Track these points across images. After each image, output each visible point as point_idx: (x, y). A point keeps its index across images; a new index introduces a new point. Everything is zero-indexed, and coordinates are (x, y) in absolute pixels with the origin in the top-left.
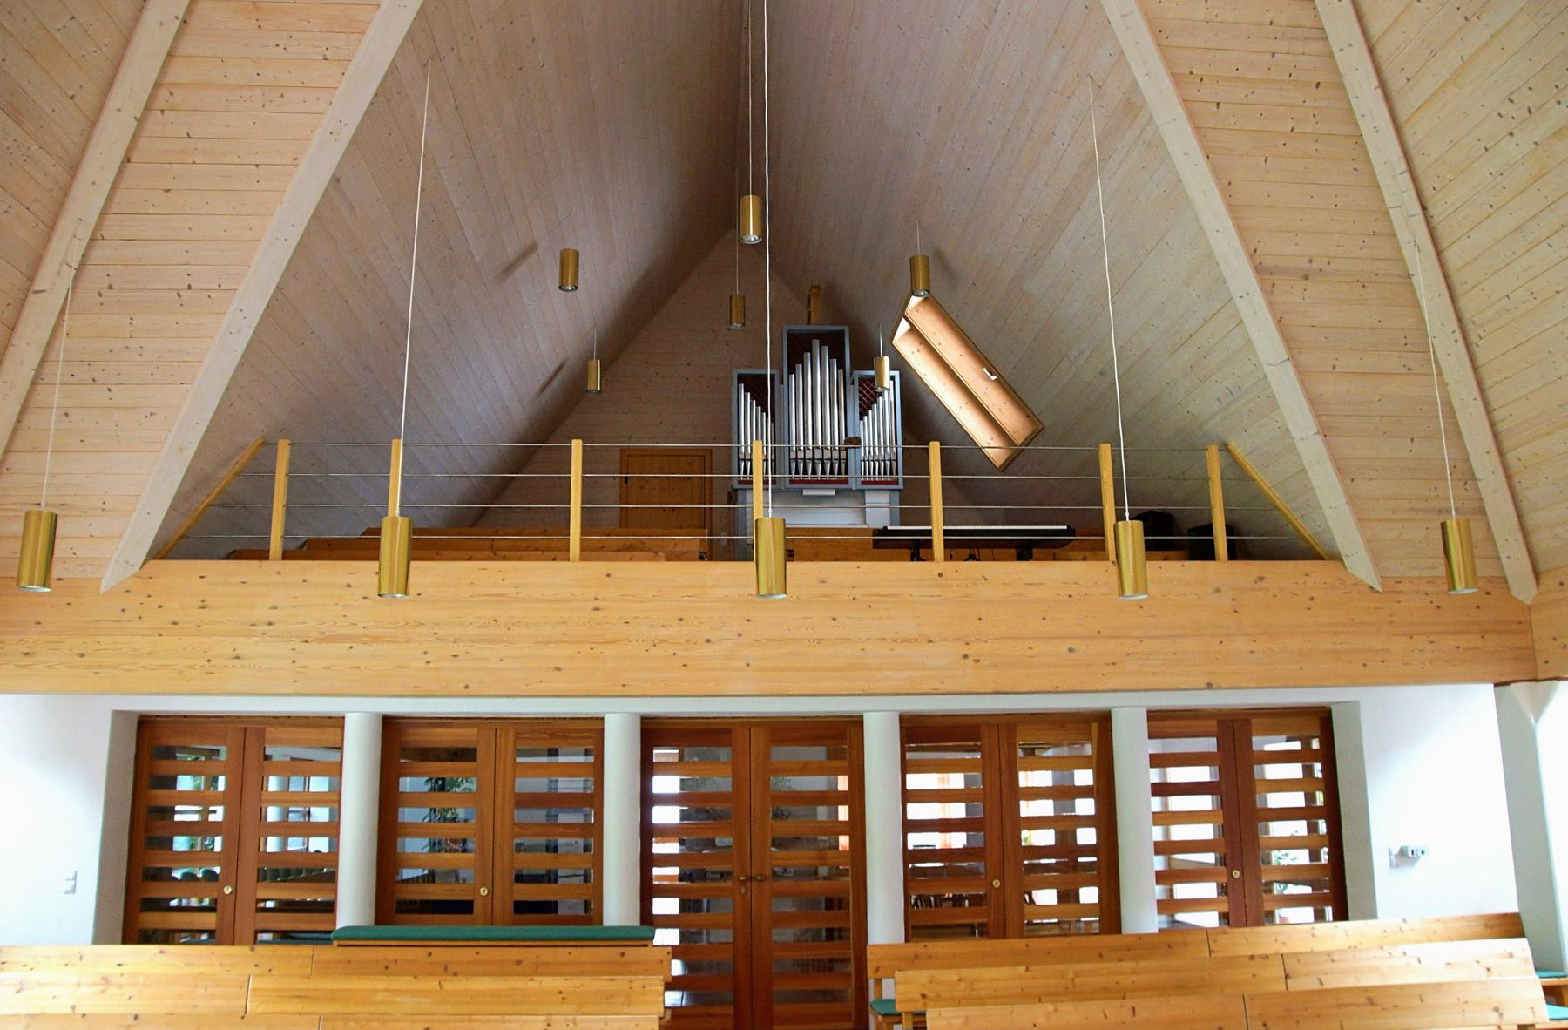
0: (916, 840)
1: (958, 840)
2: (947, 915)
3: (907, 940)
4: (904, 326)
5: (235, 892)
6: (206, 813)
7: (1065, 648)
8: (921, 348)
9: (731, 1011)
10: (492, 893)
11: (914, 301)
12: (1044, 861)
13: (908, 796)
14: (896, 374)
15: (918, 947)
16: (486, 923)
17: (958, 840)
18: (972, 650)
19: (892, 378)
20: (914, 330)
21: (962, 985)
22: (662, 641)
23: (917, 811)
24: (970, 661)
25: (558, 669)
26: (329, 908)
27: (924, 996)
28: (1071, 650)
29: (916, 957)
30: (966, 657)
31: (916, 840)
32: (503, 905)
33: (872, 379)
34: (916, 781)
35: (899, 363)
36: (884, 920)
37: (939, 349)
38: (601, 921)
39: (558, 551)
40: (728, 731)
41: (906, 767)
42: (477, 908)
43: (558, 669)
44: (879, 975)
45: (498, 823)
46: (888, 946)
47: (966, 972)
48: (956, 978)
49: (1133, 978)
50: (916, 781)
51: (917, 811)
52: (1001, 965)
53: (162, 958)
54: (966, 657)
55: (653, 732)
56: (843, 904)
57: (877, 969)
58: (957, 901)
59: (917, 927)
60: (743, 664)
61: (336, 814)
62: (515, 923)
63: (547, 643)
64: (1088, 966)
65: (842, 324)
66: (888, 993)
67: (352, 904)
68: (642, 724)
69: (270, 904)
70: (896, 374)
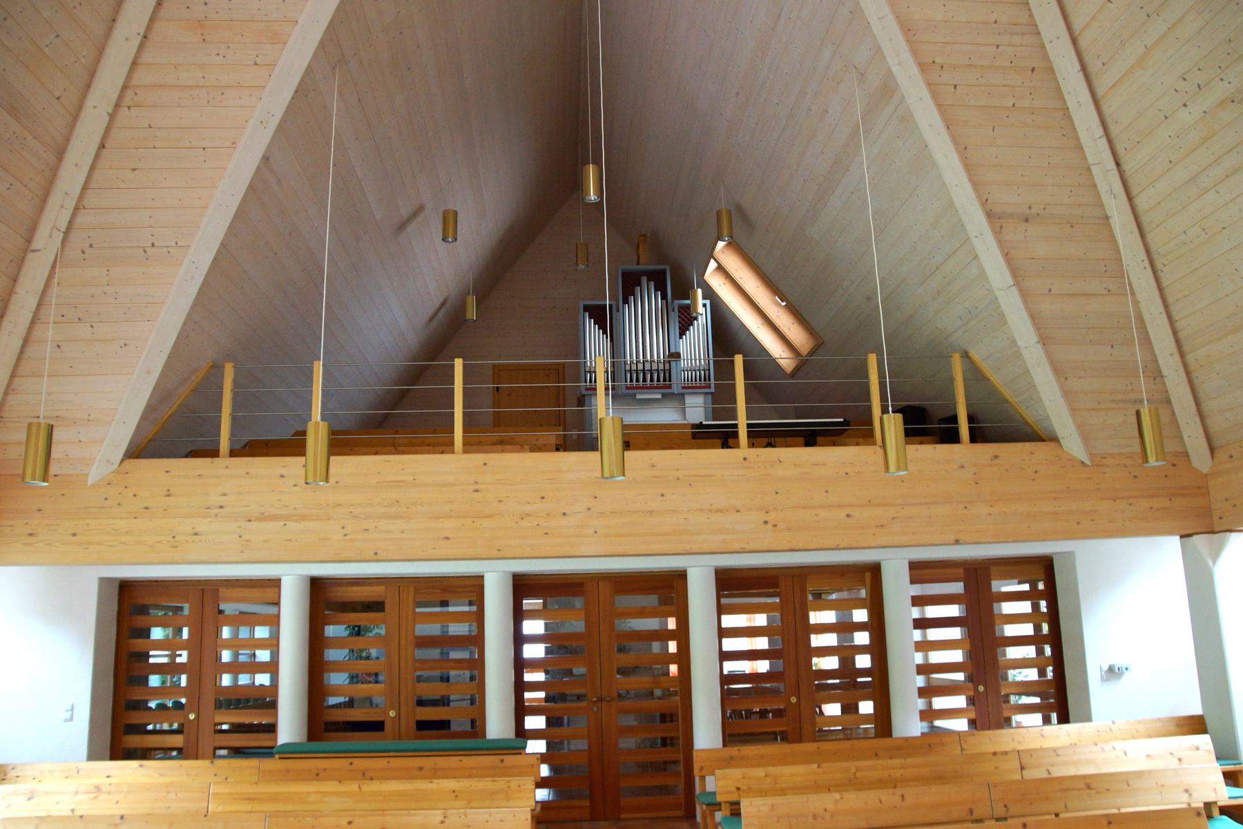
0: (730, 667)
3: (725, 745)
4: (713, 265)
6: (173, 656)
7: (843, 514)
8: (727, 282)
10: (399, 714)
11: (721, 244)
13: (723, 633)
14: (708, 302)
15: (733, 751)
17: (763, 666)
18: (771, 517)
19: (704, 305)
20: (720, 268)
21: (768, 780)
22: (528, 515)
23: (730, 644)
24: (769, 526)
25: (447, 538)
27: (738, 789)
28: (848, 516)
29: (732, 758)
30: (766, 522)
31: (730, 667)
32: (408, 724)
33: (688, 307)
34: (729, 621)
35: (710, 294)
36: (706, 730)
37: (741, 282)
39: (445, 446)
41: (721, 610)
42: (388, 727)
43: (447, 538)
46: (709, 750)
47: (773, 770)
48: (763, 774)
50: (729, 621)
51: (730, 644)
54: (766, 522)
56: (674, 718)
57: (702, 768)
59: (731, 736)
60: (592, 532)
62: (416, 738)
63: (438, 518)
65: (664, 263)
69: (225, 727)
70: (708, 302)
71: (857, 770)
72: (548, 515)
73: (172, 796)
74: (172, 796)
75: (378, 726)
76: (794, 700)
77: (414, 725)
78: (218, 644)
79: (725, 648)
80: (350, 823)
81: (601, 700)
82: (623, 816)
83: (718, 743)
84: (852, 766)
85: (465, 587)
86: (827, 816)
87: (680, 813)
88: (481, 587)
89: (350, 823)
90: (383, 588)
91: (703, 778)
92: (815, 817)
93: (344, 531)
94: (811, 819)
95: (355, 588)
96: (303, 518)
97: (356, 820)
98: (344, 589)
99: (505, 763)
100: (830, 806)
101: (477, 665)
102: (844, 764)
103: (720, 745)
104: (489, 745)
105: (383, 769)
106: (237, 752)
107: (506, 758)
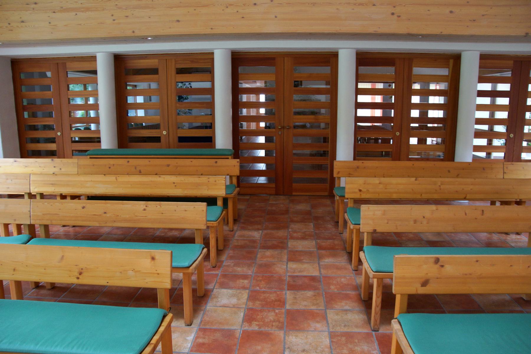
0: (362, 113)
1: (378, 113)
2: (372, 147)
3: (355, 159)
5: (62, 134)
6: (87, 100)
7: (447, 11)
9: (274, 186)
10: (168, 133)
12: (436, 125)
13: (359, 92)
15: (359, 163)
16: (167, 148)
17: (378, 113)
18: (397, 10)
21: (381, 186)
22: (231, 5)
23: (362, 99)
24: (395, 17)
25: (178, 21)
26: (98, 140)
27: (360, 191)
28: (451, 12)
29: (358, 167)
30: (393, 14)
31: (362, 113)
32: (174, 140)
34: (361, 86)
36: (344, 150)
38: (215, 147)
40: (274, 59)
41: (359, 78)
42: (162, 140)
43: (178, 21)
44: (339, 176)
45: (169, 102)
46: (345, 162)
47: (383, 180)
48: (378, 182)
49: (471, 187)
50: (361, 86)
51: (362, 99)
52: (403, 176)
53: (15, 164)
54: (393, 14)
55: (238, 60)
56: (329, 140)
57: (339, 173)
58: (376, 140)
59: (359, 153)
60: (273, 16)
61: (96, 100)
62: (179, 147)
63: (172, 8)
64: (447, 180)
66: (342, 185)
67: (107, 141)
68: (232, 55)
69: (77, 139)
71: (442, 183)
72: (244, 5)
73: (9, 181)
74: (9, 181)
75: (157, 139)
76: (398, 134)
77: (176, 140)
78: (505, 136)
79: (359, 101)
80: (83, 208)
81: (283, 128)
82: (294, 193)
83: (351, 158)
84: (439, 180)
85: (205, 59)
86: (425, 222)
87: (326, 194)
88: (212, 60)
89: (83, 208)
90: (157, 60)
91: (339, 178)
92: (415, 221)
93: (113, 18)
94: (412, 223)
95: (142, 61)
96: (88, 9)
97: (80, 208)
98: (136, 61)
99: (218, 164)
100: (428, 215)
101: (211, 105)
102: (434, 179)
103: (352, 159)
104: (216, 153)
105: (146, 166)
106: (82, 152)
107: (219, 161)
